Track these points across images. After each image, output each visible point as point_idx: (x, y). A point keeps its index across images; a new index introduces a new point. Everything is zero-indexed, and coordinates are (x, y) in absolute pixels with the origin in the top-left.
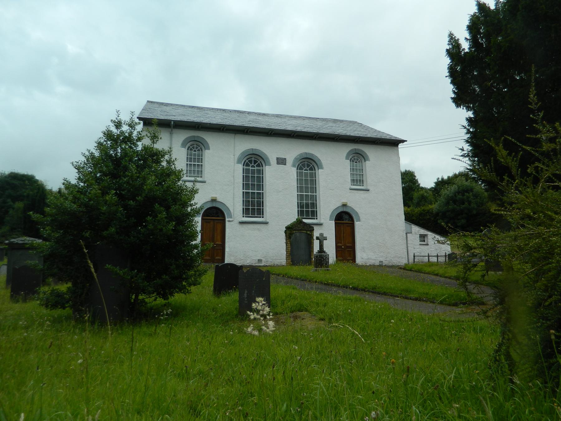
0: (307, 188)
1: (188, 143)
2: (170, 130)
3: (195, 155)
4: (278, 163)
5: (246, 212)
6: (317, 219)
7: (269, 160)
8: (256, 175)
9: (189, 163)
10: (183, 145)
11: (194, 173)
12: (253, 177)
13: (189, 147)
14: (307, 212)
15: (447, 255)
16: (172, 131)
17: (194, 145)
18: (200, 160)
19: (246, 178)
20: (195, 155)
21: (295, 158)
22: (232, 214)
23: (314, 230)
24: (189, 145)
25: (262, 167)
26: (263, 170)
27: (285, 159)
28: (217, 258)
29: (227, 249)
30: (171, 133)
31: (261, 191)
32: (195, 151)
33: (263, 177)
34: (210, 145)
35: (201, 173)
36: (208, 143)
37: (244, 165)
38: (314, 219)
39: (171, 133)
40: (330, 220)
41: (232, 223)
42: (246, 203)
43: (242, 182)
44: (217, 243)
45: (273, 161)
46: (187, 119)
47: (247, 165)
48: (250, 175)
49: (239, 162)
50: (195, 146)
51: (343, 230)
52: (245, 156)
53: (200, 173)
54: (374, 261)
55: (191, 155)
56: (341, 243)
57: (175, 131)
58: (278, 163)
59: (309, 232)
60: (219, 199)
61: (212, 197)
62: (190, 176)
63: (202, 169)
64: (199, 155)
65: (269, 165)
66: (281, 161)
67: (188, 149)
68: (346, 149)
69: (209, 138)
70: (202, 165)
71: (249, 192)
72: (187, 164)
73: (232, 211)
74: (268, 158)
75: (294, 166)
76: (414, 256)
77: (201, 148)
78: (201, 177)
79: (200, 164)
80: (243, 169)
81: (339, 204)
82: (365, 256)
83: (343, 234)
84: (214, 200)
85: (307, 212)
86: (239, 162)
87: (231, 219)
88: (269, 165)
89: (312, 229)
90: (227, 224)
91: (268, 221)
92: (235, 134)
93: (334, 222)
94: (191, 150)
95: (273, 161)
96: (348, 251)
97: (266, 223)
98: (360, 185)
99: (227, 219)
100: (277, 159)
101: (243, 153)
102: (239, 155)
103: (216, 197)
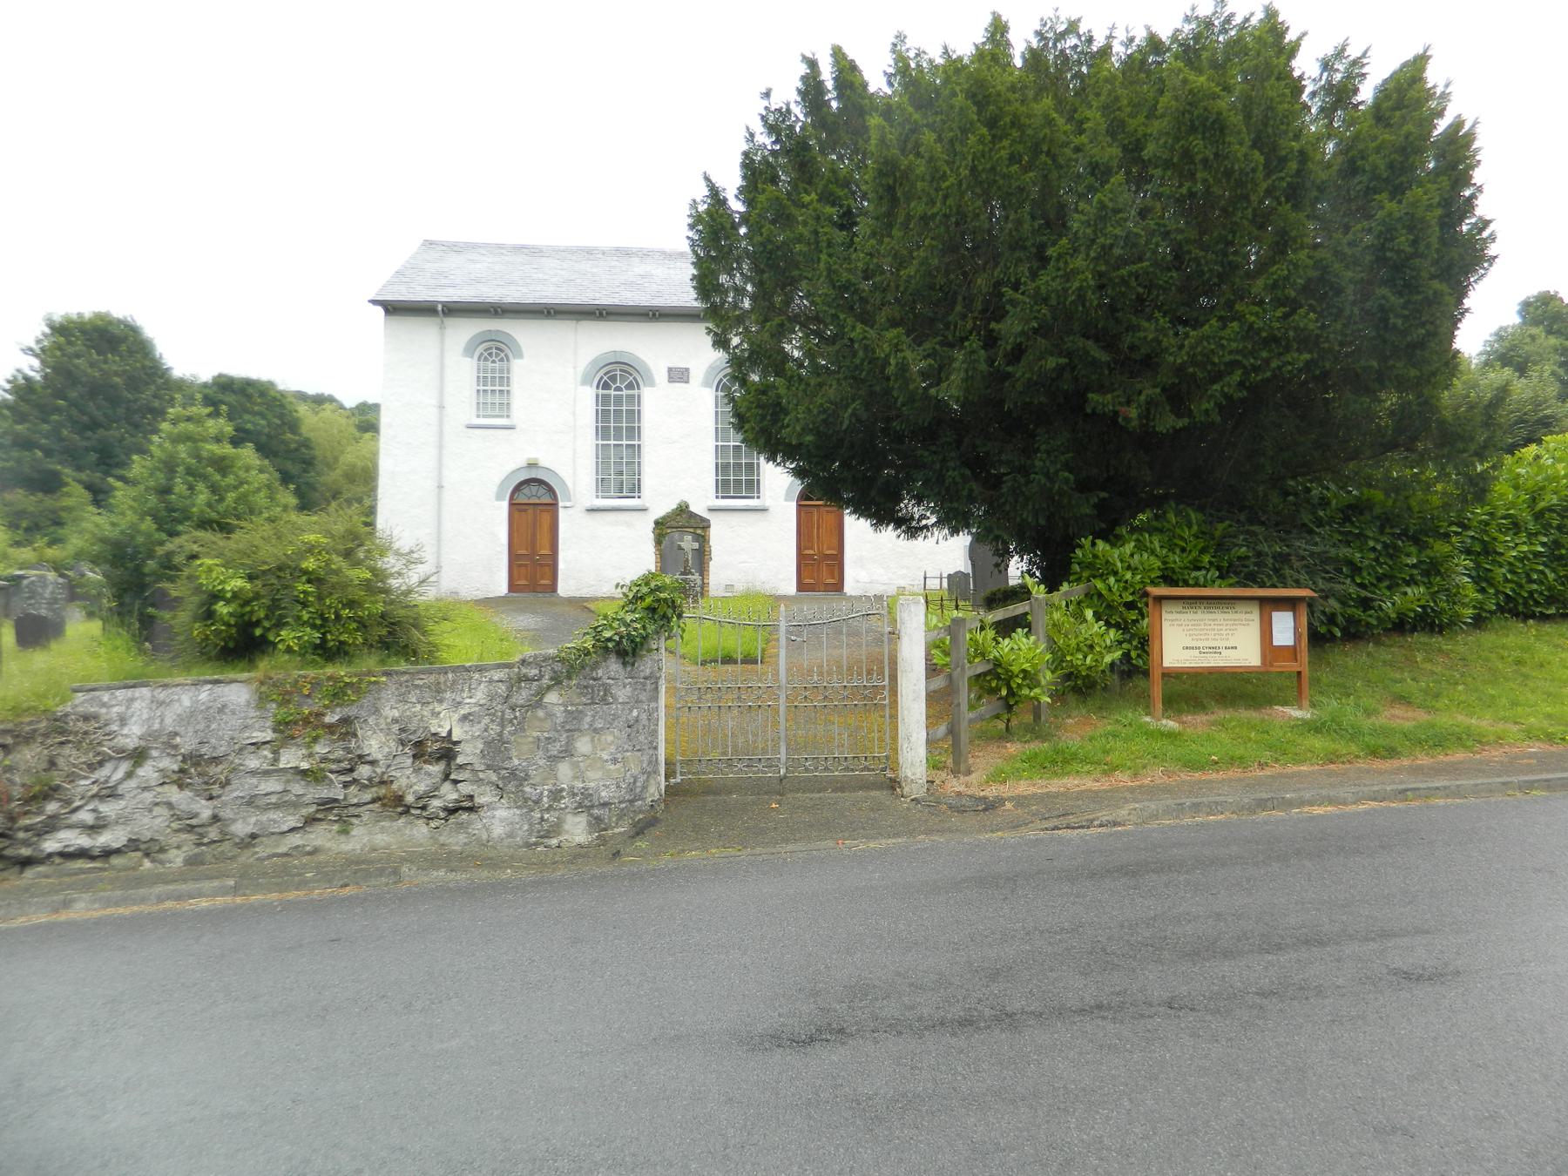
0: (618, 430)
1: (478, 345)
2: (436, 320)
3: (493, 371)
4: (671, 379)
5: (602, 485)
6: (758, 497)
7: (651, 374)
8: (624, 408)
9: (481, 388)
10: (469, 350)
11: (493, 409)
12: (618, 413)
13: (482, 354)
14: (738, 483)
15: (945, 575)
16: (442, 322)
17: (491, 348)
18: (505, 380)
19: (603, 415)
20: (493, 371)
21: (710, 367)
22: (572, 493)
23: (709, 526)
24: (480, 349)
25: (639, 388)
26: (639, 396)
27: (687, 370)
28: (542, 582)
29: (561, 566)
30: (442, 327)
31: (636, 443)
32: (494, 362)
33: (639, 411)
34: (524, 349)
35: (508, 408)
36: (519, 346)
37: (598, 387)
38: (753, 498)
39: (442, 327)
40: (786, 500)
41: (570, 511)
42: (602, 463)
43: (594, 424)
44: (542, 552)
45: (660, 375)
46: (472, 294)
47: (606, 386)
48: (612, 408)
49: (586, 381)
50: (494, 351)
51: (818, 521)
52: (598, 368)
53: (505, 408)
54: (884, 587)
55: (485, 371)
56: (812, 548)
57: (449, 321)
58: (671, 379)
59: (699, 531)
60: (543, 463)
61: (529, 459)
62: (484, 416)
63: (508, 399)
64: (501, 371)
65: (652, 383)
66: (679, 375)
67: (479, 359)
68: (464, 331)
69: (521, 332)
70: (508, 392)
71: (609, 445)
72: (478, 391)
73: (570, 485)
74: (648, 370)
75: (706, 384)
76: (925, 578)
77: (506, 355)
78: (508, 416)
79: (505, 388)
80: (597, 396)
81: (521, 462)
82: (863, 576)
83: (818, 528)
84: (532, 465)
85: (738, 483)
86: (586, 381)
87: (568, 504)
88: (652, 383)
89: (705, 524)
90: (562, 514)
91: (647, 505)
92: (578, 320)
93: (794, 504)
94: (486, 359)
95: (660, 375)
96: (828, 565)
97: (764, 510)
98: (502, 416)
99: (561, 504)
100: (670, 370)
101: (595, 361)
102: (585, 365)
103: (536, 459)
